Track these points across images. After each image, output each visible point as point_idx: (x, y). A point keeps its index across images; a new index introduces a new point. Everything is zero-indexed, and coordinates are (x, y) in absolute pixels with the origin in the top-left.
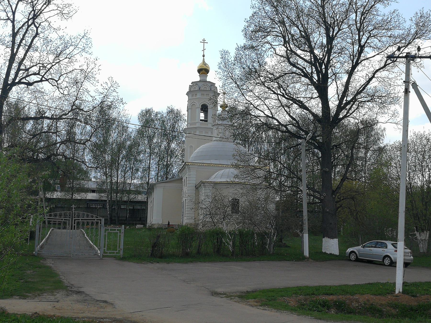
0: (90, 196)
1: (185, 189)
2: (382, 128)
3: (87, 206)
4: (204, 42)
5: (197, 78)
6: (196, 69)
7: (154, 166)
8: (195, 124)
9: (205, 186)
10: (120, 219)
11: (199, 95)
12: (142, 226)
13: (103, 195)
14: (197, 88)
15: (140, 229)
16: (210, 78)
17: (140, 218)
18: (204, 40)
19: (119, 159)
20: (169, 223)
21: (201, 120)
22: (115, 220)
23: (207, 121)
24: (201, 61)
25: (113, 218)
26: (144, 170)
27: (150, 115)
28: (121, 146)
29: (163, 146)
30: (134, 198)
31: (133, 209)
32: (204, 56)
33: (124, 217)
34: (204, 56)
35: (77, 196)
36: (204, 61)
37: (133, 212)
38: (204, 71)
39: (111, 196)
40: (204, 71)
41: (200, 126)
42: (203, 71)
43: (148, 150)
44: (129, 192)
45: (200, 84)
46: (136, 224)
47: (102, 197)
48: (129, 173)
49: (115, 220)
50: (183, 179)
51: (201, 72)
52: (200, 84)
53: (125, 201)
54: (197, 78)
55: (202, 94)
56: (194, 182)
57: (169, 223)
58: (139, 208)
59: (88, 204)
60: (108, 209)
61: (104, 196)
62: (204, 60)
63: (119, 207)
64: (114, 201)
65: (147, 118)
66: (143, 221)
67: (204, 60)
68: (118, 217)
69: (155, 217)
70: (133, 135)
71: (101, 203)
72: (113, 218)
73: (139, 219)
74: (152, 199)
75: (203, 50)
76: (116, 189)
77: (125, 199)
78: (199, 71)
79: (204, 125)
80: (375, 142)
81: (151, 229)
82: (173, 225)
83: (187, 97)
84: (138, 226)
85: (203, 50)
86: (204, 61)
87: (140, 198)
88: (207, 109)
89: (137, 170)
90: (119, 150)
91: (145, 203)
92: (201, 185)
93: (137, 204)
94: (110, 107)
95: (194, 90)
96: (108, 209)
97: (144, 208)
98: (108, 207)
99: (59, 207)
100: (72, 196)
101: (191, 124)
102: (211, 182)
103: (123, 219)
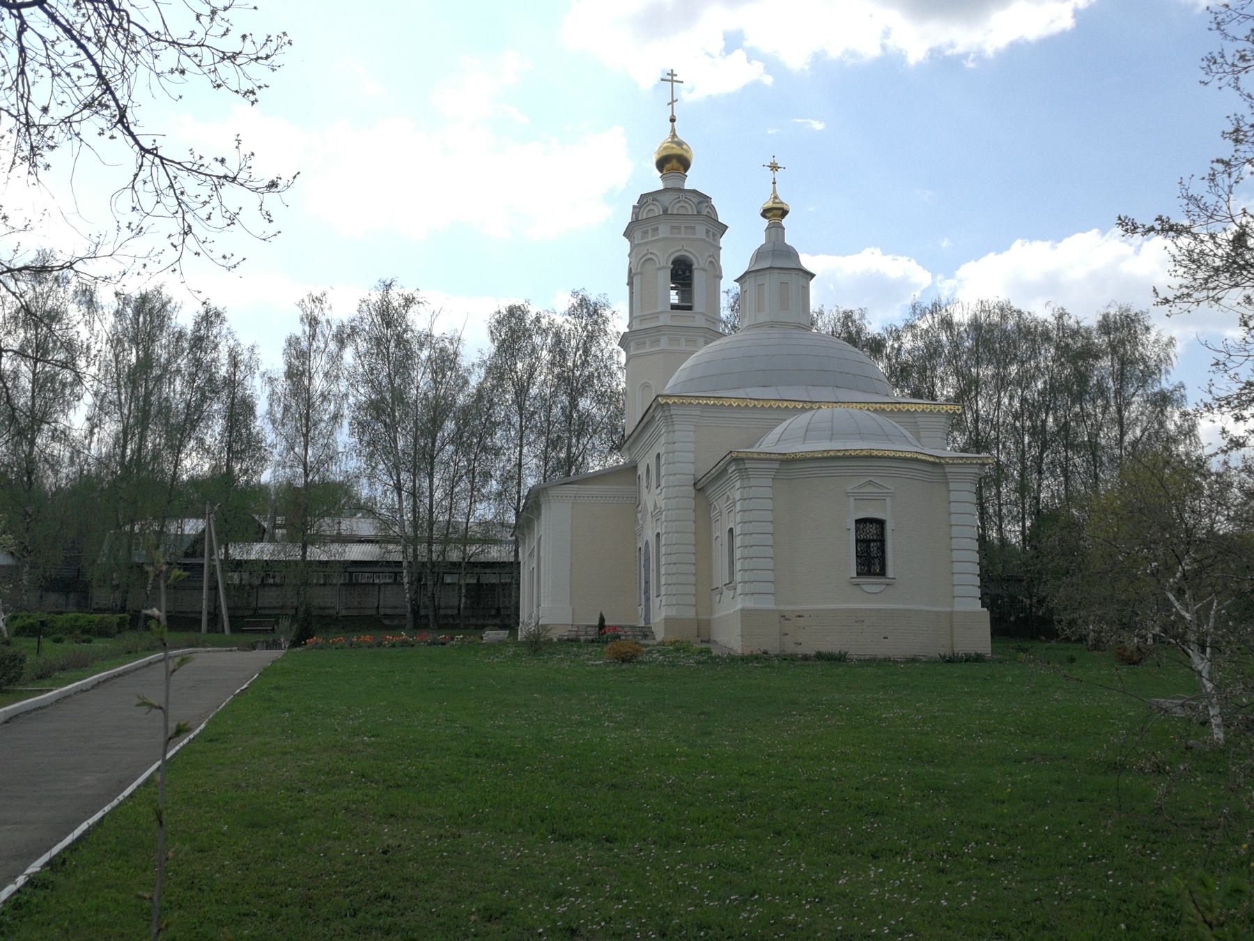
0: (355, 552)
1: (651, 498)
2: (1165, 339)
3: (351, 579)
4: (672, 81)
5: (655, 181)
6: (654, 160)
7: (531, 462)
8: (656, 316)
9: (744, 474)
10: (442, 612)
11: (664, 231)
12: (503, 634)
13: (391, 547)
14: (658, 211)
15: (497, 646)
16: (692, 181)
17: (498, 610)
18: (672, 74)
19: (433, 445)
20: (602, 619)
21: (674, 307)
22: (427, 616)
23: (690, 308)
24: (668, 134)
25: (422, 612)
26: (505, 480)
27: (521, 319)
28: (439, 410)
29: (556, 410)
30: (478, 554)
31: (479, 585)
32: (673, 120)
33: (452, 608)
34: (673, 120)
35: (317, 553)
36: (674, 135)
37: (478, 592)
38: (674, 163)
39: (415, 550)
40: (674, 163)
41: (669, 323)
42: (673, 162)
43: (516, 419)
44: (466, 540)
45: (667, 199)
46: (483, 627)
47: (390, 552)
48: (464, 484)
49: (427, 616)
50: (642, 470)
51: (668, 166)
52: (667, 199)
53: (453, 564)
54: (655, 181)
55: (672, 227)
56: (691, 468)
57: (602, 619)
58: (494, 581)
59: (351, 573)
60: (406, 586)
61: (395, 553)
62: (673, 130)
63: (439, 581)
64: (424, 564)
65: (513, 330)
66: (508, 618)
67: (673, 130)
68: (437, 609)
69: (547, 602)
70: (474, 381)
71: (386, 570)
72: (422, 612)
73: (493, 612)
74: (535, 544)
75: (672, 103)
76: (423, 529)
77: (455, 555)
78: (662, 164)
79: (683, 318)
80: (1149, 374)
81: (538, 645)
82: (614, 628)
83: (626, 244)
84: (491, 635)
85: (672, 103)
86: (674, 135)
87: (494, 553)
88: (691, 272)
89: (487, 476)
90: (436, 422)
91: (513, 567)
92: (725, 470)
93: (488, 571)
94: (409, 301)
95: (647, 219)
96: (406, 586)
97: (508, 581)
98: (406, 580)
99: (272, 585)
100: (304, 553)
101: (643, 319)
102: (767, 458)
103: (450, 612)
